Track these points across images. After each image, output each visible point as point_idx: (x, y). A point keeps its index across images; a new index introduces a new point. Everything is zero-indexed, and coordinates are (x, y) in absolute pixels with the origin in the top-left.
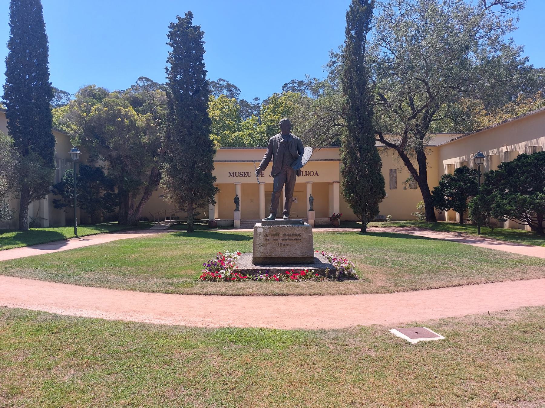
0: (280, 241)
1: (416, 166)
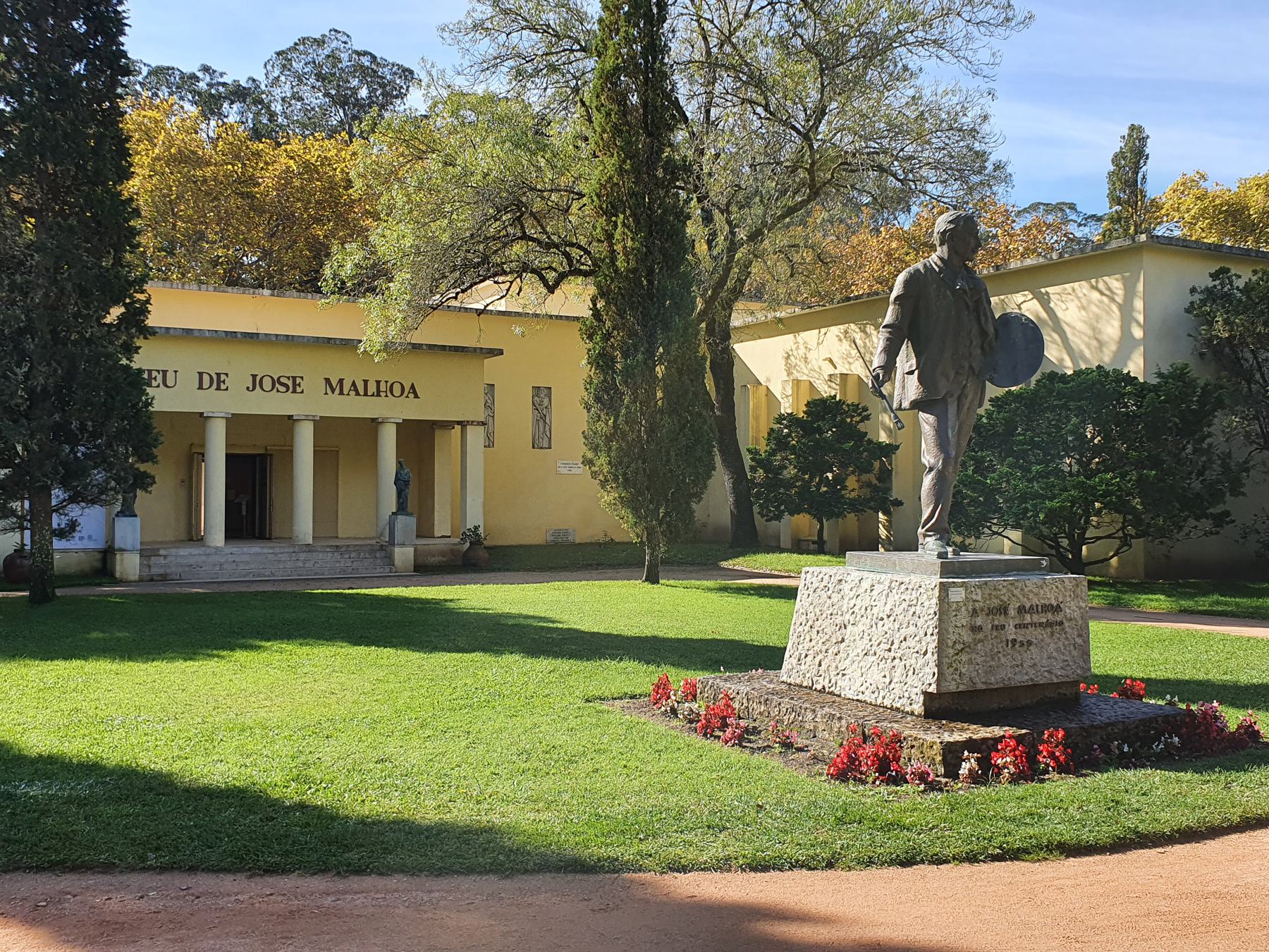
0: (1011, 632)
1: (1107, 292)
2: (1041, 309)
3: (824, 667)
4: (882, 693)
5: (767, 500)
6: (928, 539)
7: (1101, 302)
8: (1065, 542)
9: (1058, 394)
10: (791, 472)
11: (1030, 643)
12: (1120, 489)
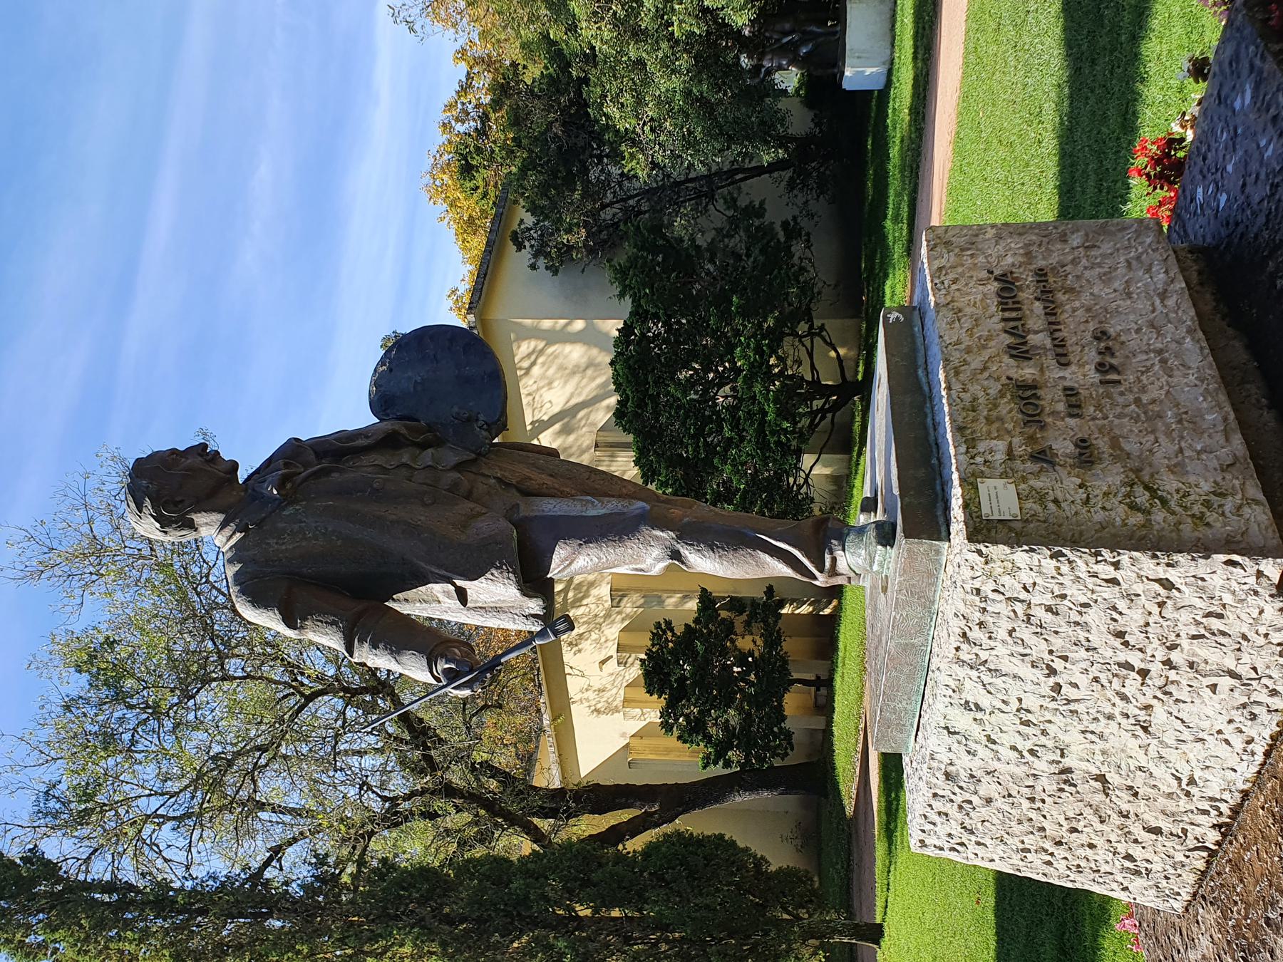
0: (1083, 374)
1: (533, 357)
2: (551, 430)
3: (1165, 825)
4: (1262, 697)
5: (766, 747)
6: (842, 565)
7: (543, 364)
8: (817, 404)
9: (638, 406)
10: (733, 716)
11: (1101, 335)
12: (754, 336)
